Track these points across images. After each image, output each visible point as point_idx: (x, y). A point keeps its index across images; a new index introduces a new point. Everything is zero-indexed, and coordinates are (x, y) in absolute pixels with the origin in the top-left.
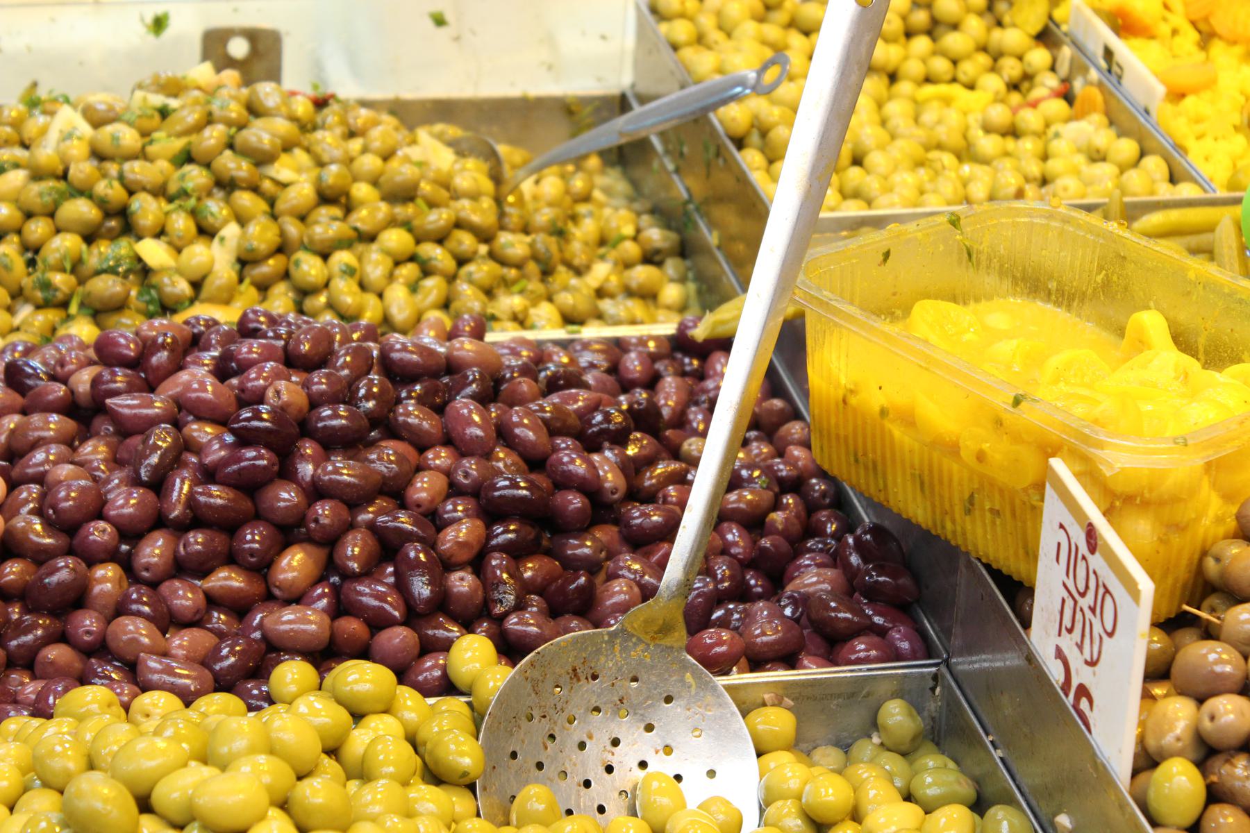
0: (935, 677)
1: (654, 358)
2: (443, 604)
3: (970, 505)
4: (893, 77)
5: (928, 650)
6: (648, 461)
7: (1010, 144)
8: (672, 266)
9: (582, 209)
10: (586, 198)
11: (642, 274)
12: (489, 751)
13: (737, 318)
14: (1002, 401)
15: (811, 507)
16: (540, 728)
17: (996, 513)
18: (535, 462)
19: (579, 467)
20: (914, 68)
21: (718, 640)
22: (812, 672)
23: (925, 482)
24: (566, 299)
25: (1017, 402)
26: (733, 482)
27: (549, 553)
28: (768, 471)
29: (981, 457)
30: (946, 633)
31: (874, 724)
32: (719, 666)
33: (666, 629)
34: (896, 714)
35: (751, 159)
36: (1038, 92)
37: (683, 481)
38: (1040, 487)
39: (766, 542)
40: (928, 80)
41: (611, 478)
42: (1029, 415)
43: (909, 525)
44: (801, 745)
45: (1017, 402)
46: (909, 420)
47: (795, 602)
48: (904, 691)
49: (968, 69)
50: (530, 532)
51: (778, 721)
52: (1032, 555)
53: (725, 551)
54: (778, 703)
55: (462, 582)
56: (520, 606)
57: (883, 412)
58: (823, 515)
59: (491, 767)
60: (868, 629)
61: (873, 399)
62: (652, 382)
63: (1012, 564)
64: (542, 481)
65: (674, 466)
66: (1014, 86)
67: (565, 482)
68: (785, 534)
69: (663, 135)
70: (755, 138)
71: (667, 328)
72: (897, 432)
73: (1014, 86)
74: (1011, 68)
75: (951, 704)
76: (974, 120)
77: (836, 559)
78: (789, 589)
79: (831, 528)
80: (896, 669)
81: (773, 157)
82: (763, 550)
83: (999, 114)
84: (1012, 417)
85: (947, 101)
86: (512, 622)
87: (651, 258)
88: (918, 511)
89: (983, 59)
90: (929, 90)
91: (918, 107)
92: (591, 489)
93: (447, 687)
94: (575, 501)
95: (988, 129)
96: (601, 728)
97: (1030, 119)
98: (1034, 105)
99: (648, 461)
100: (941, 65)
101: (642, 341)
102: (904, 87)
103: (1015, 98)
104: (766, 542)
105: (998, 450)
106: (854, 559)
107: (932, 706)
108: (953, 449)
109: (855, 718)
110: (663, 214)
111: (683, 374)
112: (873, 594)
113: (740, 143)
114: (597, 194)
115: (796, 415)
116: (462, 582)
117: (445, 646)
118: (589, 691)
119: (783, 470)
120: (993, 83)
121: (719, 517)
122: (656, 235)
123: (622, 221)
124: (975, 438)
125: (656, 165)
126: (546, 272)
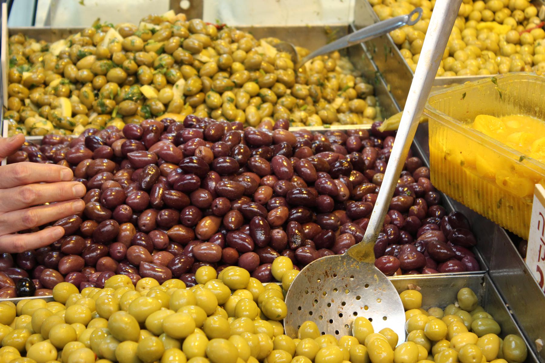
0: (483, 279)
1: (361, 139)
2: (270, 243)
3: (500, 204)
4: (467, 19)
5: (479, 266)
6: (358, 183)
7: (518, 48)
8: (370, 100)
9: (331, 75)
10: (333, 70)
11: (357, 103)
12: (289, 306)
13: (399, 122)
14: (515, 158)
15: (429, 204)
16: (311, 297)
17: (511, 208)
18: (310, 182)
19: (329, 185)
20: (476, 15)
21: (389, 260)
22: (429, 275)
23: (480, 193)
24: (324, 113)
25: (521, 159)
26: (395, 192)
27: (315, 222)
28: (411, 188)
29: (505, 183)
30: (488, 260)
31: (456, 299)
32: (389, 272)
33: (366, 255)
34: (465, 294)
35: (405, 54)
36: (531, 26)
37: (374, 192)
38: (531, 197)
39: (409, 219)
40: (482, 20)
41: (343, 190)
42: (527, 165)
43: (472, 212)
44: (424, 307)
45: (521, 159)
46: (473, 167)
47: (422, 245)
48: (470, 284)
49: (500, 15)
50: (308, 213)
51: (414, 296)
52: (527, 226)
53: (391, 222)
54: (414, 288)
55: (278, 234)
56: (303, 245)
57: (462, 163)
58: (434, 208)
59: (290, 313)
60: (453, 257)
61: (458, 157)
62: (361, 149)
63: (518, 230)
64: (313, 191)
65: (370, 185)
66: (520, 23)
67: (323, 191)
68: (418, 215)
69: (366, 43)
70: (407, 45)
71: (368, 126)
72: (468, 172)
73: (520, 23)
74: (519, 15)
75: (490, 290)
76: (502, 38)
77: (440, 227)
78: (419, 239)
79: (438, 213)
80: (466, 275)
81: (415, 52)
82: (408, 222)
83: (514, 35)
84: (519, 166)
85: (491, 29)
86: (300, 251)
87: (361, 96)
88: (476, 206)
89: (507, 11)
90: (483, 24)
91: (478, 32)
92: (334, 194)
93: (271, 278)
94: (327, 200)
95: (508, 42)
96: (338, 297)
97: (528, 37)
98: (529, 31)
99: (358, 183)
100: (488, 14)
101: (357, 132)
102: (472, 23)
103: (521, 28)
104: (409, 219)
105: (512, 180)
106: (448, 227)
107: (481, 291)
108: (493, 180)
109: (448, 295)
110: (366, 77)
111: (374, 146)
112: (456, 242)
113: (400, 47)
114: (338, 69)
115: (423, 165)
116: (278, 234)
117: (271, 261)
118: (332, 281)
119: (417, 188)
120: (511, 22)
121: (389, 208)
122: (363, 86)
123: (348, 80)
124: (503, 175)
125: (363, 56)
126: (316, 102)
